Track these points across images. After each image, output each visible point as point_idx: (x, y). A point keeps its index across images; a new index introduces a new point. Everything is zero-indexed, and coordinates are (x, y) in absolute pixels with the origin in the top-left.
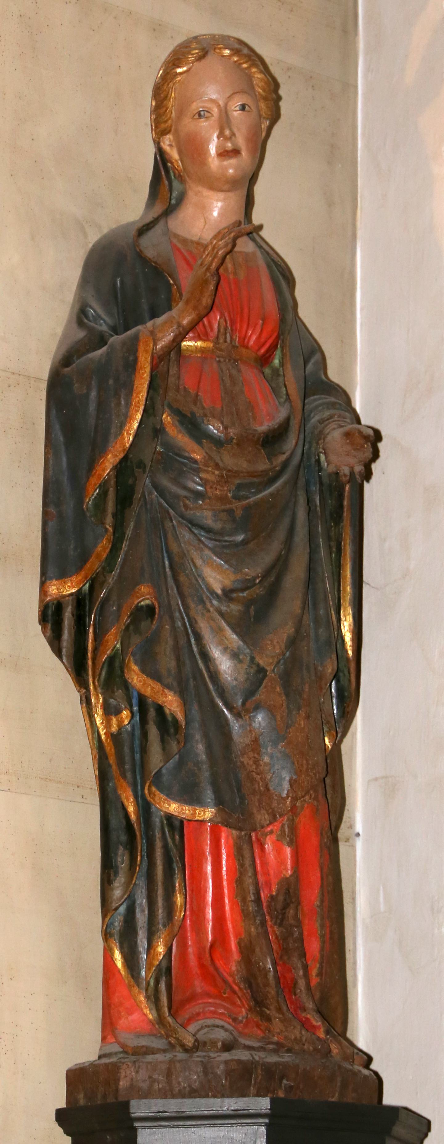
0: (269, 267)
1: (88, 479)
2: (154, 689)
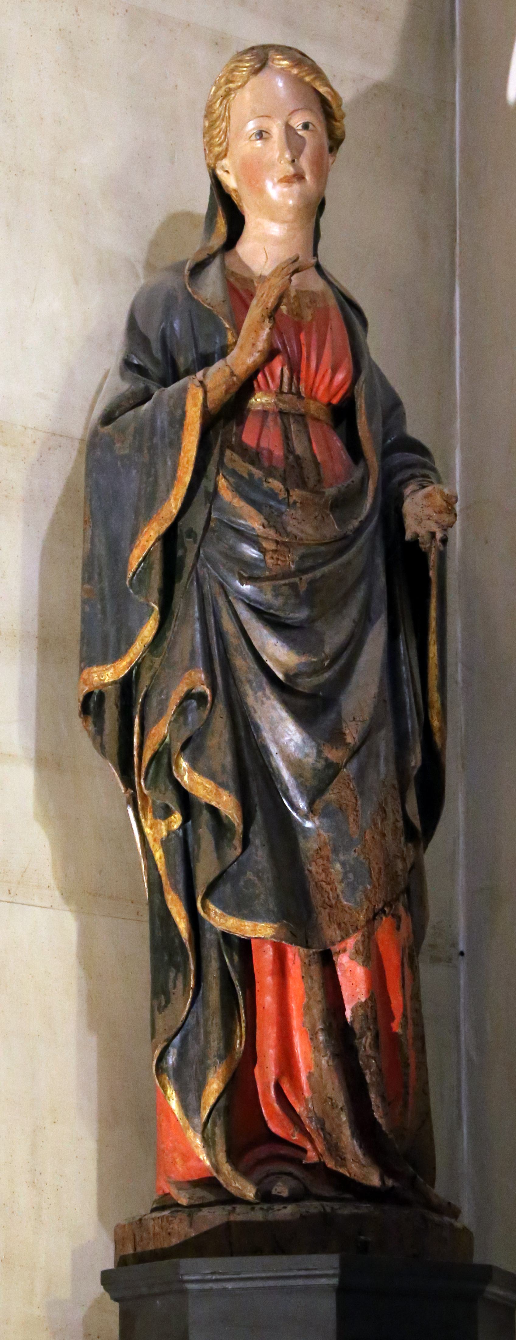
0: (342, 309)
1: (131, 551)
2: (207, 789)
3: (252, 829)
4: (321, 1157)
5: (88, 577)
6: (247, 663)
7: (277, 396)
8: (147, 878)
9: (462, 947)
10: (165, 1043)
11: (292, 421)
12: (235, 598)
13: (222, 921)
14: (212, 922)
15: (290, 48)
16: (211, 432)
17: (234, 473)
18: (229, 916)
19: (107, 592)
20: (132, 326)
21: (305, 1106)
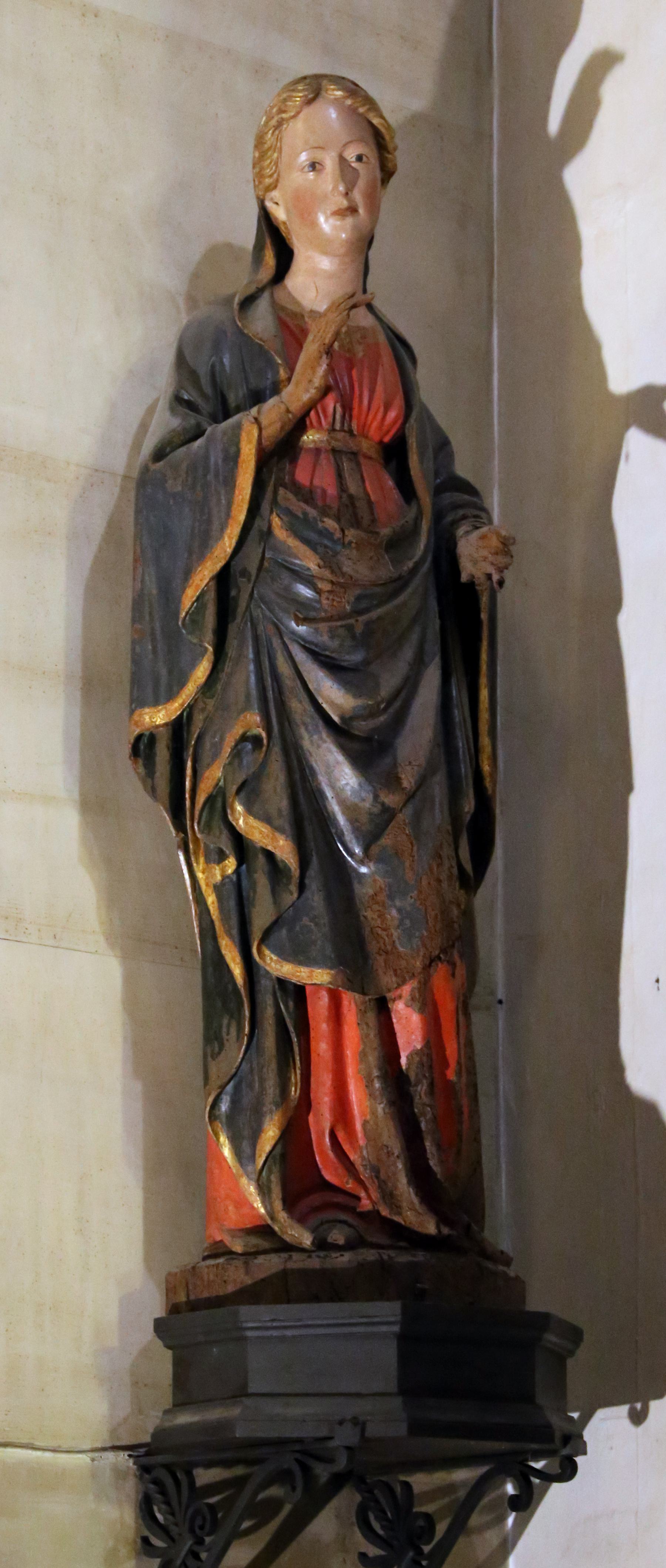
2: (263, 833)
3: (308, 874)
4: (375, 1204)
5: (136, 618)
6: (303, 706)
7: (329, 433)
8: (198, 923)
9: (500, 994)
10: (219, 1090)
11: (344, 459)
12: (290, 639)
13: (278, 967)
14: (268, 968)
15: (343, 78)
16: (265, 470)
17: (289, 512)
18: (284, 963)
19: (158, 632)
20: (181, 360)
21: (359, 1153)
